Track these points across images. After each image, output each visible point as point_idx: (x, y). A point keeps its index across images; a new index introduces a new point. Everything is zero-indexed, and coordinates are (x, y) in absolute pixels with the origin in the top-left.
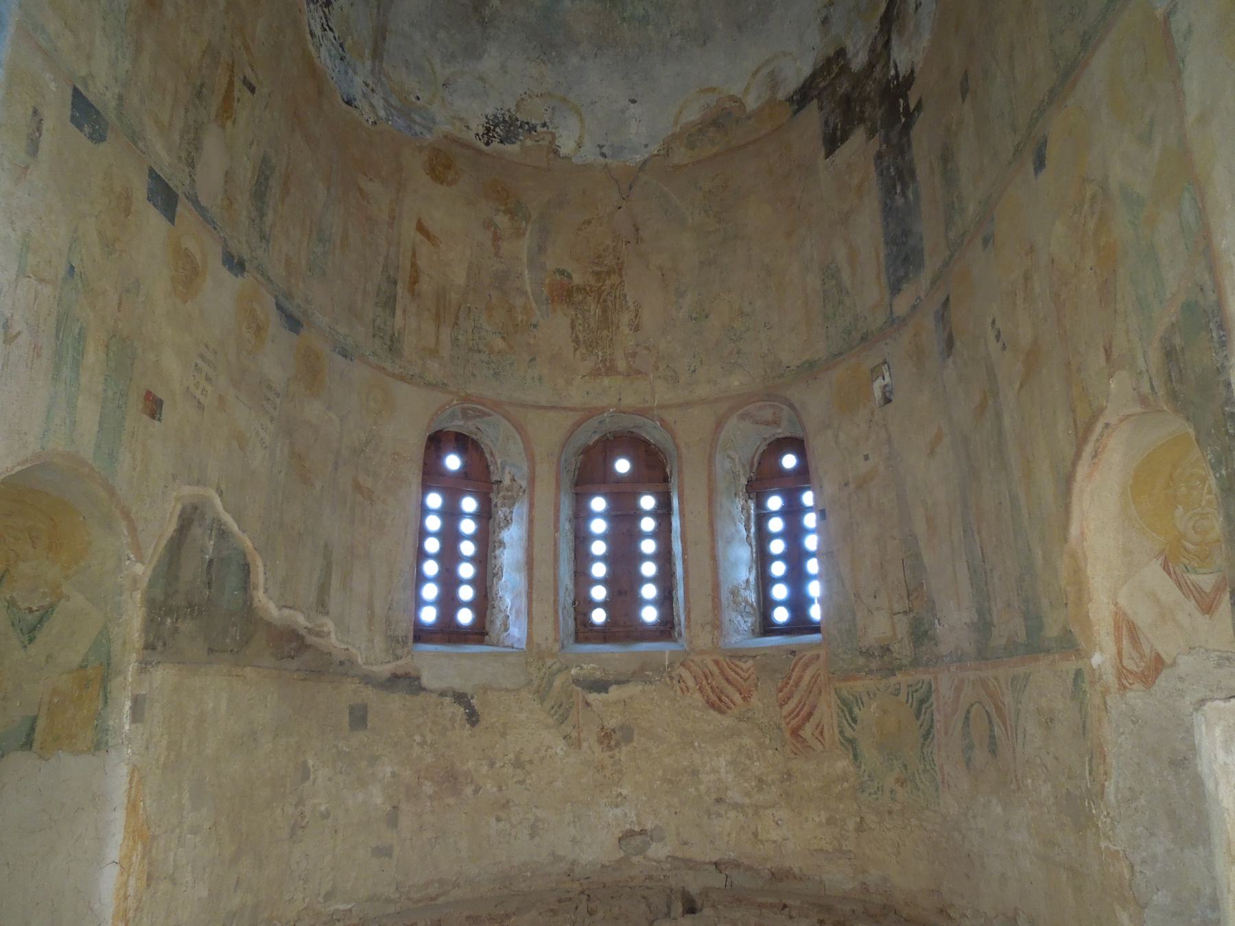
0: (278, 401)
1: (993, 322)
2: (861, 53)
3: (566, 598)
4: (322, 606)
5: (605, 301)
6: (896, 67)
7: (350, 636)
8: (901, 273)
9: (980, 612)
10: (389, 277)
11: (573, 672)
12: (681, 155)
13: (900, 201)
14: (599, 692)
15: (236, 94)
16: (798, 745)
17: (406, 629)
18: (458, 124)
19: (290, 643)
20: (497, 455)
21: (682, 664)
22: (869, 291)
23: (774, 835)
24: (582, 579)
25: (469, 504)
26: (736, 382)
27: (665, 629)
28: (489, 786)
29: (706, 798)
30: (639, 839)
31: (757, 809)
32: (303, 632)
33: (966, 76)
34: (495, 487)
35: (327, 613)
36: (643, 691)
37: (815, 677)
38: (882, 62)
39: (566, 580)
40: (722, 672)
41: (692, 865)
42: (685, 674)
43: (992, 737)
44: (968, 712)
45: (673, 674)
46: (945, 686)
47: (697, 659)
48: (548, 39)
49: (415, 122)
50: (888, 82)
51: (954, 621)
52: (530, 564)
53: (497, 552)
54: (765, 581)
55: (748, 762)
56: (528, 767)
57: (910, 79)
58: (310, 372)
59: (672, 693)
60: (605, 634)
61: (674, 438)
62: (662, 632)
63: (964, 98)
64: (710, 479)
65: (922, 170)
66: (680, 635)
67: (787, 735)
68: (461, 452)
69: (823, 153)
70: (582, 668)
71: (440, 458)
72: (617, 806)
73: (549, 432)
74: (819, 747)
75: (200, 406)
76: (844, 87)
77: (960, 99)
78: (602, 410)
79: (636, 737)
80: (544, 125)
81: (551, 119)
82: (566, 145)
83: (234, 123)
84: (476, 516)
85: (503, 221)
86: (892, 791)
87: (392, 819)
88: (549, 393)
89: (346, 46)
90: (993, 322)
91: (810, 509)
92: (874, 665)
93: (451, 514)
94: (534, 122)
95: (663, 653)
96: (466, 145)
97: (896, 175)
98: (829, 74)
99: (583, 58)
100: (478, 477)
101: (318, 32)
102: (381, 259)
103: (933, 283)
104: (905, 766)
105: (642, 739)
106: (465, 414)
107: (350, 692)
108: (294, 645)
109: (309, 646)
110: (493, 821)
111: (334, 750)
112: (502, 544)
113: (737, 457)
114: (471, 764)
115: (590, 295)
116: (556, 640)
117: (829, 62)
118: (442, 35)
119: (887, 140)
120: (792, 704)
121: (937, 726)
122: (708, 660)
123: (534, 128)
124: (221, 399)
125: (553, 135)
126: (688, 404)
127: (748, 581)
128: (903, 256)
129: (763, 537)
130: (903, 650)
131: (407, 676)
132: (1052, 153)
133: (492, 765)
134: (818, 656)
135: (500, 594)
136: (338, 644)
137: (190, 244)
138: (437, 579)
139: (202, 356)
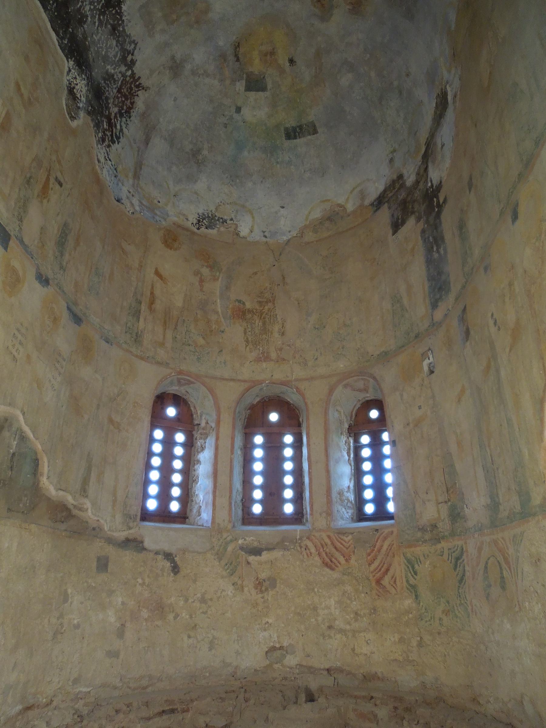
0: (64, 363)
1: (492, 315)
2: (411, 176)
3: (237, 497)
4: (84, 492)
5: (264, 318)
6: (431, 181)
7: (101, 512)
8: (438, 296)
9: (492, 498)
10: (137, 299)
11: (240, 542)
12: (310, 236)
13: (436, 255)
14: (256, 555)
15: (51, 186)
16: (380, 590)
17: (136, 510)
18: (181, 217)
19: (62, 513)
20: (198, 408)
21: (308, 538)
22: (419, 309)
23: (365, 650)
24: (248, 486)
25: (180, 437)
26: (341, 365)
27: (298, 517)
28: (184, 614)
29: (323, 626)
30: (279, 652)
31: (355, 632)
32: (71, 507)
33: (471, 179)
34: (196, 427)
35: (87, 497)
36: (283, 555)
37: (391, 545)
38: (423, 180)
39: (238, 485)
40: (333, 544)
41: (311, 670)
42: (310, 544)
43: (502, 578)
44: (487, 563)
45: (302, 544)
46: (471, 549)
47: (317, 534)
48: (235, 174)
49: (156, 214)
50: (427, 190)
51: (476, 505)
52: (215, 474)
53: (196, 467)
54: (359, 488)
55: (348, 602)
56: (210, 603)
57: (440, 186)
58: (86, 349)
59: (301, 557)
60: (261, 520)
61: (304, 399)
62: (296, 519)
63: (470, 191)
64: (325, 423)
65: (448, 237)
66: (307, 521)
67: (374, 584)
68: (174, 406)
69: (391, 232)
70: (245, 540)
71: (163, 409)
72: (265, 630)
73: (229, 394)
74: (393, 591)
75: (15, 359)
76: (402, 195)
77: (468, 192)
78: (261, 382)
79: (278, 585)
80: (232, 220)
81: (236, 216)
82: (244, 231)
83: (48, 201)
84: (184, 445)
85: (205, 271)
86: (440, 619)
87: (121, 633)
88: (230, 372)
89: (118, 170)
90: (492, 315)
91: (388, 457)
92: (427, 536)
93: (168, 443)
94: (225, 218)
95: (296, 531)
96: (187, 229)
97: (434, 240)
98: (394, 189)
99: (254, 183)
100: (186, 421)
101: (102, 160)
102: (133, 289)
103: (457, 299)
104: (448, 602)
105: (282, 586)
106: (179, 382)
107: (99, 547)
108: (64, 514)
109: (74, 516)
110: (185, 638)
111: (85, 584)
112: (199, 462)
113: (342, 411)
114: (173, 599)
115: (255, 315)
116: (230, 521)
117: (394, 182)
118: (174, 168)
119: (427, 222)
120: (376, 563)
121: (467, 574)
122: (324, 535)
123: (225, 221)
124: (28, 357)
125: (236, 225)
126: (312, 379)
127: (349, 487)
128: (438, 286)
129: (358, 460)
130: (445, 526)
131: (135, 540)
132: (522, 210)
133: (186, 600)
134: (392, 532)
135: (197, 493)
136: (92, 517)
137: (16, 264)
138: (158, 483)
139: (18, 330)
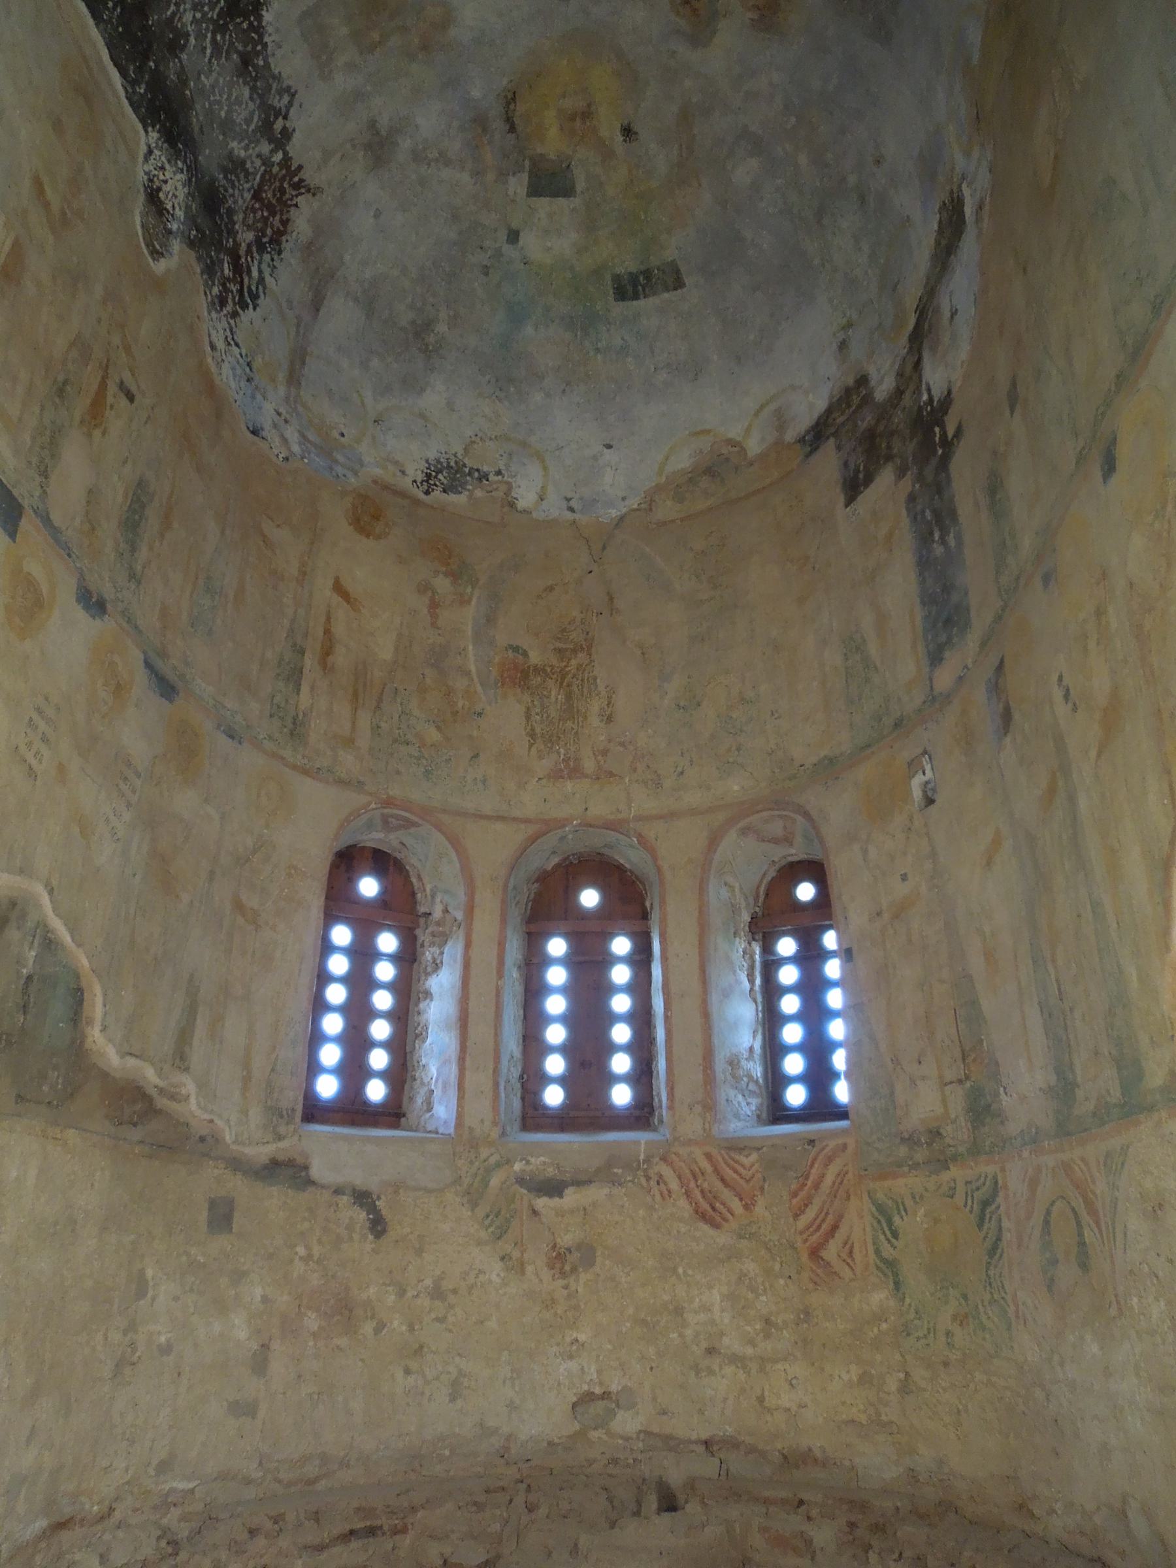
0: (138, 782)
1: (1060, 679)
2: (886, 379)
3: (511, 1071)
4: (180, 1059)
5: (569, 685)
6: (929, 390)
7: (217, 1103)
8: (943, 638)
9: (1059, 1072)
10: (295, 645)
11: (517, 1167)
12: (667, 509)
13: (939, 550)
14: (551, 1196)
15: (110, 400)
16: (819, 1271)
17: (293, 1099)
18: (391, 467)
19: (133, 1106)
20: (426, 880)
21: (664, 1159)
22: (903, 665)
23: (787, 1399)
24: (534, 1046)
25: (387, 942)
26: (735, 787)
27: (642, 1113)
28: (396, 1323)
29: (695, 1348)
30: (601, 1404)
31: (764, 1362)
32: (153, 1092)
33: (1014, 385)
34: (422, 921)
35: (187, 1069)
36: (610, 1196)
37: (842, 1175)
38: (912, 387)
39: (512, 1044)
40: (716, 1171)
41: (671, 1444)
42: (667, 1172)
43: (1082, 1244)
44: (1048, 1213)
45: (651, 1173)
46: (1015, 1181)
47: (683, 1151)
48: (505, 374)
49: (336, 461)
50: (920, 409)
51: (1025, 1087)
52: (463, 1021)
53: (422, 1006)
54: (774, 1050)
55: (750, 1296)
56: (451, 1298)
57: (947, 401)
58: (185, 752)
59: (649, 1199)
60: (562, 1120)
61: (655, 859)
62: (638, 1118)
63: (1012, 412)
64: (701, 912)
65: (964, 510)
66: (661, 1121)
67: (805, 1257)
68: (375, 874)
69: (842, 499)
70: (528, 1162)
71: (351, 881)
72: (571, 1357)
73: (494, 849)
74: (847, 1273)
75: (31, 773)
76: (867, 420)
77: (1007, 413)
78: (561, 823)
79: (599, 1260)
80: (499, 473)
81: (507, 466)
82: (526, 497)
83: (104, 434)
84: (396, 958)
85: (443, 584)
86: (948, 1334)
87: (260, 1363)
88: (495, 802)
89: (255, 366)
90: (1060, 679)
91: (835, 984)
92: (920, 1155)
93: (363, 954)
94: (485, 469)
95: (637, 1143)
96: (403, 494)
97: (934, 518)
98: (849, 406)
99: (548, 395)
100: (402, 908)
101: (220, 345)
102: (286, 622)
103: (983, 644)
104: (965, 1297)
105: (607, 1262)
106: (386, 824)
107: (212, 1178)
108: (138, 1107)
109: (158, 1112)
110: (399, 1374)
111: (184, 1258)
112: (428, 995)
113: (737, 885)
114: (372, 1290)
115: (550, 678)
116: (495, 1123)
117: (848, 391)
118: (375, 363)
119: (920, 478)
120: (811, 1213)
121: (1007, 1236)
122: (698, 1153)
123: (485, 476)
124: (61, 769)
125: (509, 485)
126: (672, 816)
127: (751, 1049)
128: (944, 616)
129: (771, 991)
130: (958, 1133)
131: (290, 1163)
132: (1123, 453)
133: (402, 1293)
134: (845, 1147)
135: (424, 1061)
136: (198, 1113)
137: (34, 568)
138: (340, 1039)
139: (39, 711)
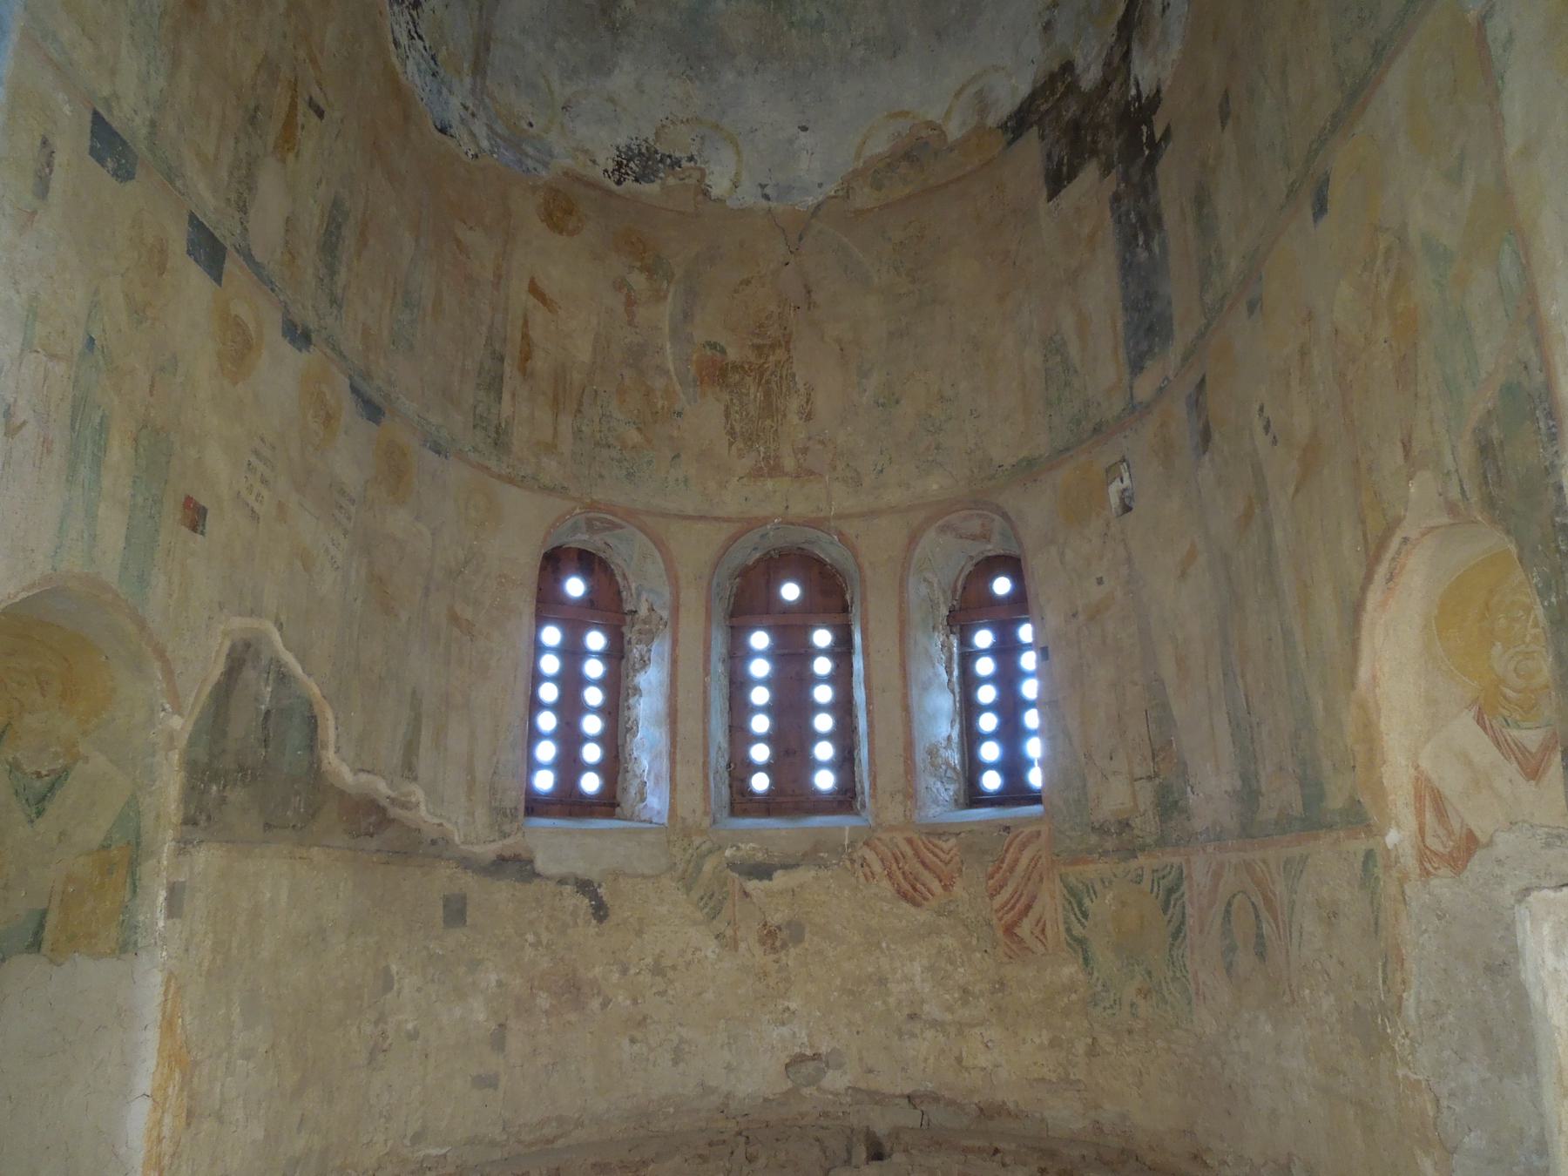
0: (353, 509)
1: (1261, 409)
2: (1093, 68)
3: (719, 760)
4: (409, 769)
5: (768, 382)
6: (1137, 85)
7: (444, 808)
8: (1144, 346)
9: (1245, 778)
10: (494, 352)
11: (728, 853)
12: (865, 197)
13: (1143, 255)
14: (761, 878)
15: (300, 119)
16: (1014, 947)
17: (515, 799)
18: (581, 157)
19: (368, 817)
20: (631, 578)
21: (866, 844)
22: (1103, 370)
23: (983, 1060)
24: (740, 735)
25: (596, 640)
26: (934, 485)
27: (845, 799)
28: (620, 998)
29: (897, 1013)
30: (811, 1065)
31: (961, 1027)
32: (385, 803)
33: (1226, 97)
34: (628, 618)
35: (415, 779)
36: (817, 878)
37: (1035, 860)
38: (1120, 79)
39: (719, 736)
40: (917, 854)
41: (878, 1098)
42: (870, 856)
43: (1260, 936)
44: (1229, 904)
45: (855, 856)
46: (1199, 871)
47: (885, 836)
48: (695, 50)
49: (527, 155)
50: (1128, 104)
51: (1211, 788)
52: (673, 717)
53: (631, 701)
54: (971, 738)
55: (949, 968)
56: (670, 974)
57: (1155, 100)
58: (394, 472)
59: (853, 880)
60: (768, 806)
61: (856, 557)
62: (840, 802)
63: (1223, 125)
64: (901, 609)
65: (1170, 216)
66: (863, 806)
67: (1000, 934)
68: (586, 574)
69: (1044, 194)
70: (738, 848)
71: (558, 581)
72: (783, 1024)
73: (697, 549)
74: (1040, 949)
75: (254, 516)
76: (1071, 110)
77: (1219, 126)
78: (765, 521)
79: (807, 936)
80: (691, 159)
81: (700, 151)
82: (719, 184)
83: (297, 156)
84: (604, 656)
85: (638, 280)
86: (1132, 1005)
87: (498, 1040)
88: (697, 499)
89: (439, 58)
90: (1261, 409)
91: (1028, 647)
92: (1110, 844)
93: (573, 653)
94: (677, 154)
95: (841, 829)
96: (592, 185)
97: (1138, 223)
98: (1053, 94)
99: (740, 74)
100: (607, 606)
101: (404, 40)
102: (484, 329)
103: (1185, 359)
104: (1149, 973)
105: (815, 938)
106: (590, 526)
107: (445, 878)
108: (373, 819)
109: (393, 821)
110: (626, 1042)
111: (424, 953)
112: (637, 691)
113: (935, 581)
114: (597, 971)
115: (750, 375)
116: (706, 813)
117: (1052, 78)
118: (561, 44)
119: (1126, 177)
120: (1005, 894)
121: (1190, 921)
122: (899, 839)
123: (677, 163)
124: (281, 506)
125: (702, 171)
126: (873, 513)
127: (949, 738)
128: (1146, 325)
129: (969, 682)
130: (1146, 825)
131: (516, 858)
132: (1336, 194)
133: (624, 971)
134: (1039, 834)
135: (635, 754)
136: (429, 818)
137: (241, 310)
138: (555, 736)
139: (256, 453)
